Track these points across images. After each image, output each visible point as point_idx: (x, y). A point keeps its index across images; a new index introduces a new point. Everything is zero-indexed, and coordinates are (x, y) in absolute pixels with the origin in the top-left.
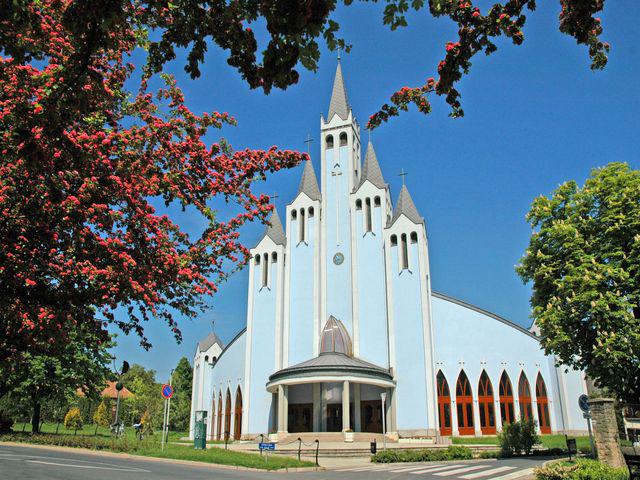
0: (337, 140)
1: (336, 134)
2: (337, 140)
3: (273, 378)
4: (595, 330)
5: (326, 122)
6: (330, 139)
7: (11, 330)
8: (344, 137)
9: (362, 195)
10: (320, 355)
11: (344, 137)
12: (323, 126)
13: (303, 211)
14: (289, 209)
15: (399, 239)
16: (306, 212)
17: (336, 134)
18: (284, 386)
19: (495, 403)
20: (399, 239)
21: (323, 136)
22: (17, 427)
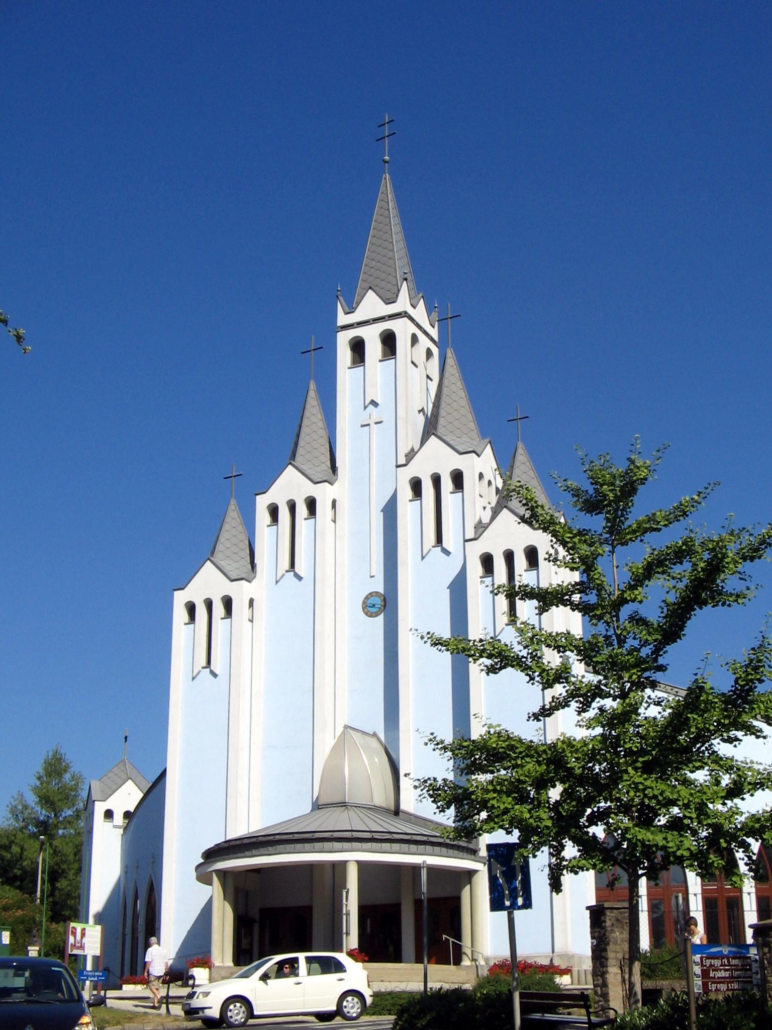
0: (373, 349)
1: (372, 337)
2: (373, 349)
3: (211, 855)
4: (636, 812)
5: (350, 311)
6: (358, 347)
7: (548, 597)
8: (389, 341)
9: (422, 468)
10: (312, 811)
11: (389, 341)
12: (343, 319)
13: (436, 480)
14: (262, 502)
15: (201, 612)
16: (447, 484)
17: (372, 337)
18: (217, 872)
19: (745, 898)
20: (201, 612)
21: (343, 339)
22: (625, 778)
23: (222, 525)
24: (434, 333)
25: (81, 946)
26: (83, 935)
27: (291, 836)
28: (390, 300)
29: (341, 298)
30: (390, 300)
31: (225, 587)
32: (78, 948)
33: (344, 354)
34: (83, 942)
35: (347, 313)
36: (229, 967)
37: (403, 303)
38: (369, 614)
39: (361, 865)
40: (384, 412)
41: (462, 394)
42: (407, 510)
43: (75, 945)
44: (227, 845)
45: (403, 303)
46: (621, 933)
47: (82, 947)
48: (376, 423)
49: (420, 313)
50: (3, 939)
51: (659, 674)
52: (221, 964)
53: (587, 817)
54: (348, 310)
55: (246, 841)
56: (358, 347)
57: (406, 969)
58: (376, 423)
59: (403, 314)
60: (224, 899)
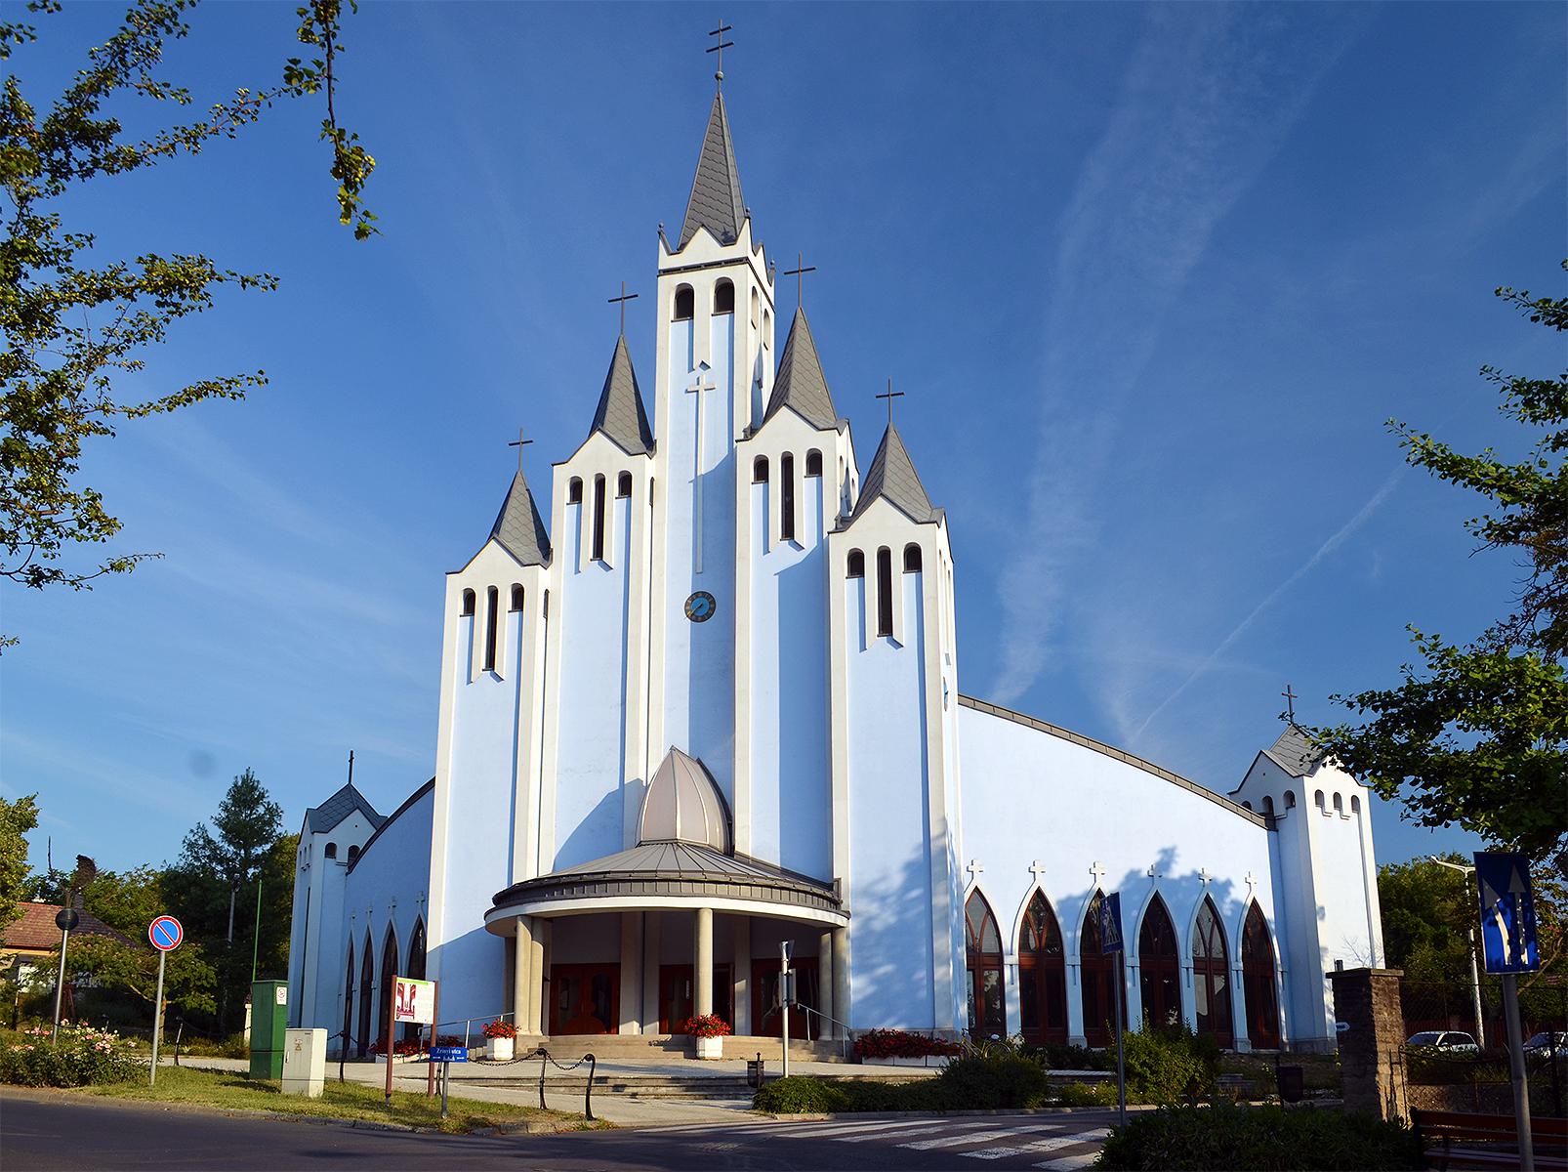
0: (705, 299)
1: (704, 288)
2: (705, 299)
6: (685, 302)
8: (725, 295)
11: (725, 295)
17: (704, 288)
18: (532, 921)
19: (1069, 970)
23: (200, 1069)
24: (770, 291)
25: (410, 1011)
26: (413, 995)
27: (628, 874)
28: (728, 240)
30: (728, 240)
31: (620, 462)
32: (406, 1013)
34: (413, 1004)
36: (537, 1037)
37: (743, 246)
38: (712, 606)
39: (718, 915)
40: (718, 376)
42: (748, 493)
43: (402, 1010)
44: (538, 883)
45: (743, 246)
46: (1390, 1014)
47: (411, 1012)
50: (278, 998)
51: (1499, 517)
52: (528, 1033)
53: (174, 1000)
56: (685, 302)
57: (764, 1044)
59: (744, 261)
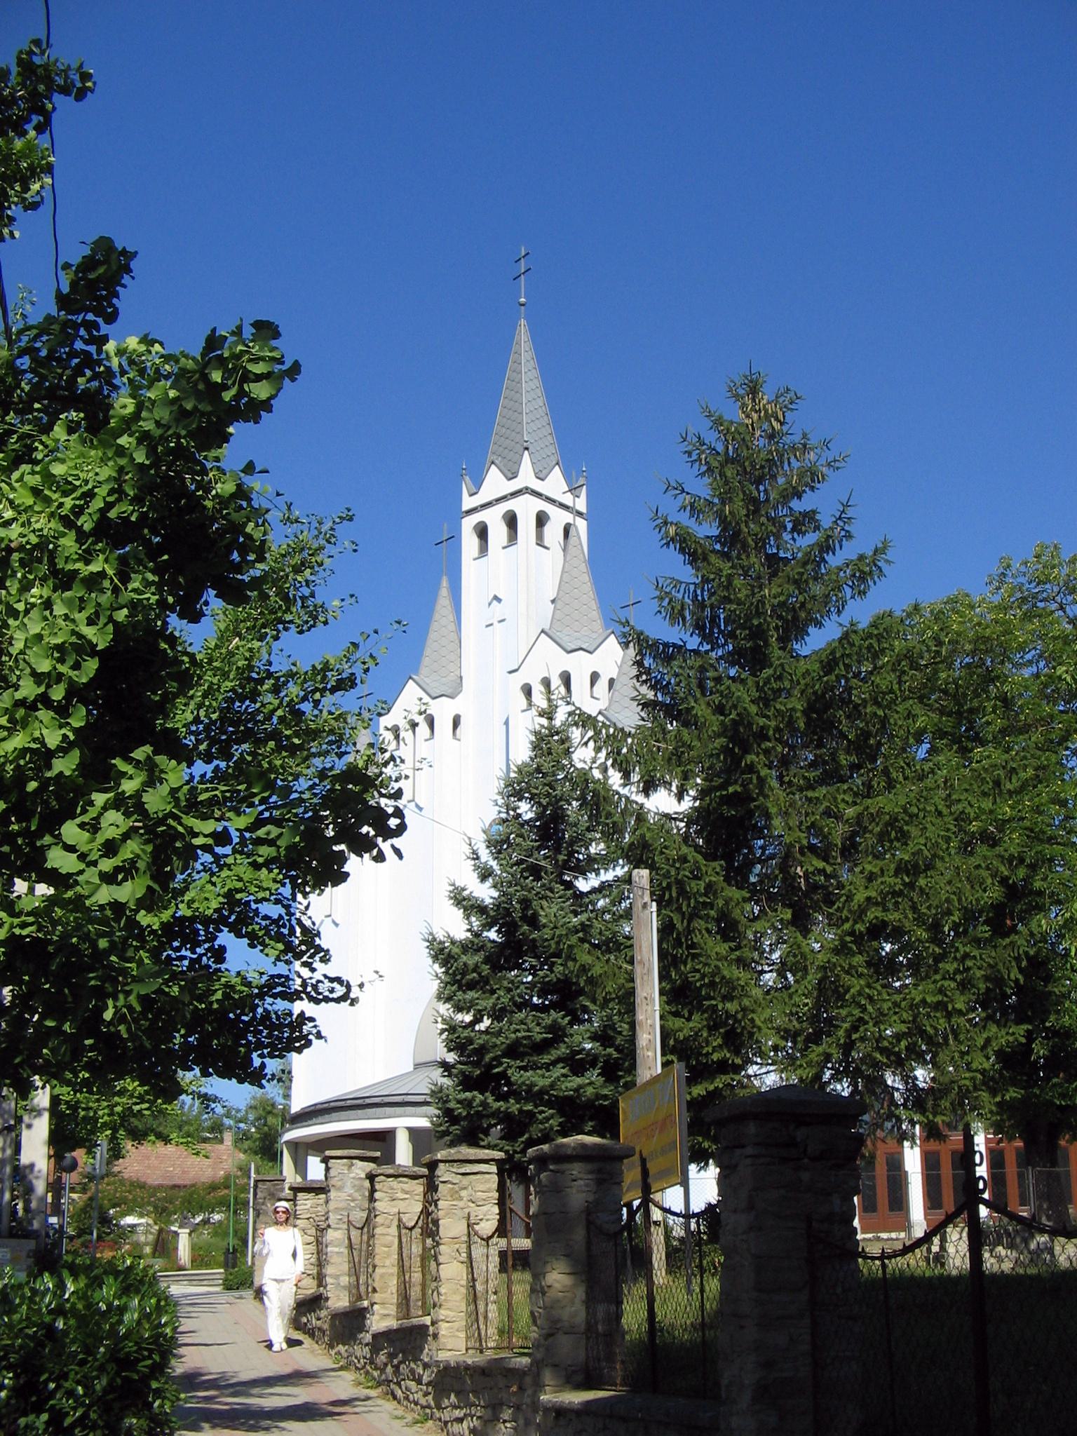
0: (498, 532)
1: (494, 519)
2: (526, 526)
6: (482, 532)
11: (511, 521)
12: (468, 502)
21: (468, 524)
28: (512, 475)
29: (467, 478)
33: (469, 542)
35: (510, 479)
37: (527, 476)
41: (586, 578)
48: (500, 622)
49: (555, 484)
54: (511, 476)
55: (318, 1107)
56: (482, 532)
58: (500, 622)
60: (296, 1172)
